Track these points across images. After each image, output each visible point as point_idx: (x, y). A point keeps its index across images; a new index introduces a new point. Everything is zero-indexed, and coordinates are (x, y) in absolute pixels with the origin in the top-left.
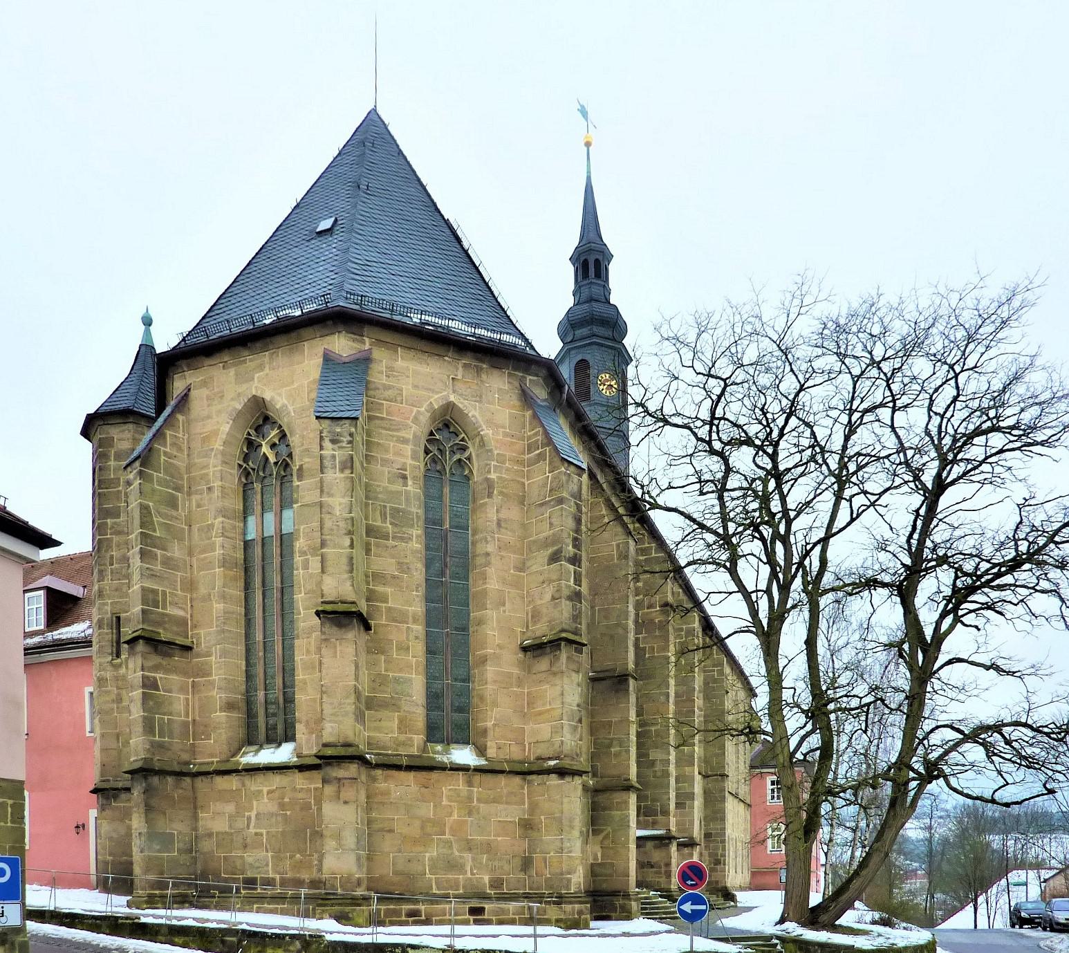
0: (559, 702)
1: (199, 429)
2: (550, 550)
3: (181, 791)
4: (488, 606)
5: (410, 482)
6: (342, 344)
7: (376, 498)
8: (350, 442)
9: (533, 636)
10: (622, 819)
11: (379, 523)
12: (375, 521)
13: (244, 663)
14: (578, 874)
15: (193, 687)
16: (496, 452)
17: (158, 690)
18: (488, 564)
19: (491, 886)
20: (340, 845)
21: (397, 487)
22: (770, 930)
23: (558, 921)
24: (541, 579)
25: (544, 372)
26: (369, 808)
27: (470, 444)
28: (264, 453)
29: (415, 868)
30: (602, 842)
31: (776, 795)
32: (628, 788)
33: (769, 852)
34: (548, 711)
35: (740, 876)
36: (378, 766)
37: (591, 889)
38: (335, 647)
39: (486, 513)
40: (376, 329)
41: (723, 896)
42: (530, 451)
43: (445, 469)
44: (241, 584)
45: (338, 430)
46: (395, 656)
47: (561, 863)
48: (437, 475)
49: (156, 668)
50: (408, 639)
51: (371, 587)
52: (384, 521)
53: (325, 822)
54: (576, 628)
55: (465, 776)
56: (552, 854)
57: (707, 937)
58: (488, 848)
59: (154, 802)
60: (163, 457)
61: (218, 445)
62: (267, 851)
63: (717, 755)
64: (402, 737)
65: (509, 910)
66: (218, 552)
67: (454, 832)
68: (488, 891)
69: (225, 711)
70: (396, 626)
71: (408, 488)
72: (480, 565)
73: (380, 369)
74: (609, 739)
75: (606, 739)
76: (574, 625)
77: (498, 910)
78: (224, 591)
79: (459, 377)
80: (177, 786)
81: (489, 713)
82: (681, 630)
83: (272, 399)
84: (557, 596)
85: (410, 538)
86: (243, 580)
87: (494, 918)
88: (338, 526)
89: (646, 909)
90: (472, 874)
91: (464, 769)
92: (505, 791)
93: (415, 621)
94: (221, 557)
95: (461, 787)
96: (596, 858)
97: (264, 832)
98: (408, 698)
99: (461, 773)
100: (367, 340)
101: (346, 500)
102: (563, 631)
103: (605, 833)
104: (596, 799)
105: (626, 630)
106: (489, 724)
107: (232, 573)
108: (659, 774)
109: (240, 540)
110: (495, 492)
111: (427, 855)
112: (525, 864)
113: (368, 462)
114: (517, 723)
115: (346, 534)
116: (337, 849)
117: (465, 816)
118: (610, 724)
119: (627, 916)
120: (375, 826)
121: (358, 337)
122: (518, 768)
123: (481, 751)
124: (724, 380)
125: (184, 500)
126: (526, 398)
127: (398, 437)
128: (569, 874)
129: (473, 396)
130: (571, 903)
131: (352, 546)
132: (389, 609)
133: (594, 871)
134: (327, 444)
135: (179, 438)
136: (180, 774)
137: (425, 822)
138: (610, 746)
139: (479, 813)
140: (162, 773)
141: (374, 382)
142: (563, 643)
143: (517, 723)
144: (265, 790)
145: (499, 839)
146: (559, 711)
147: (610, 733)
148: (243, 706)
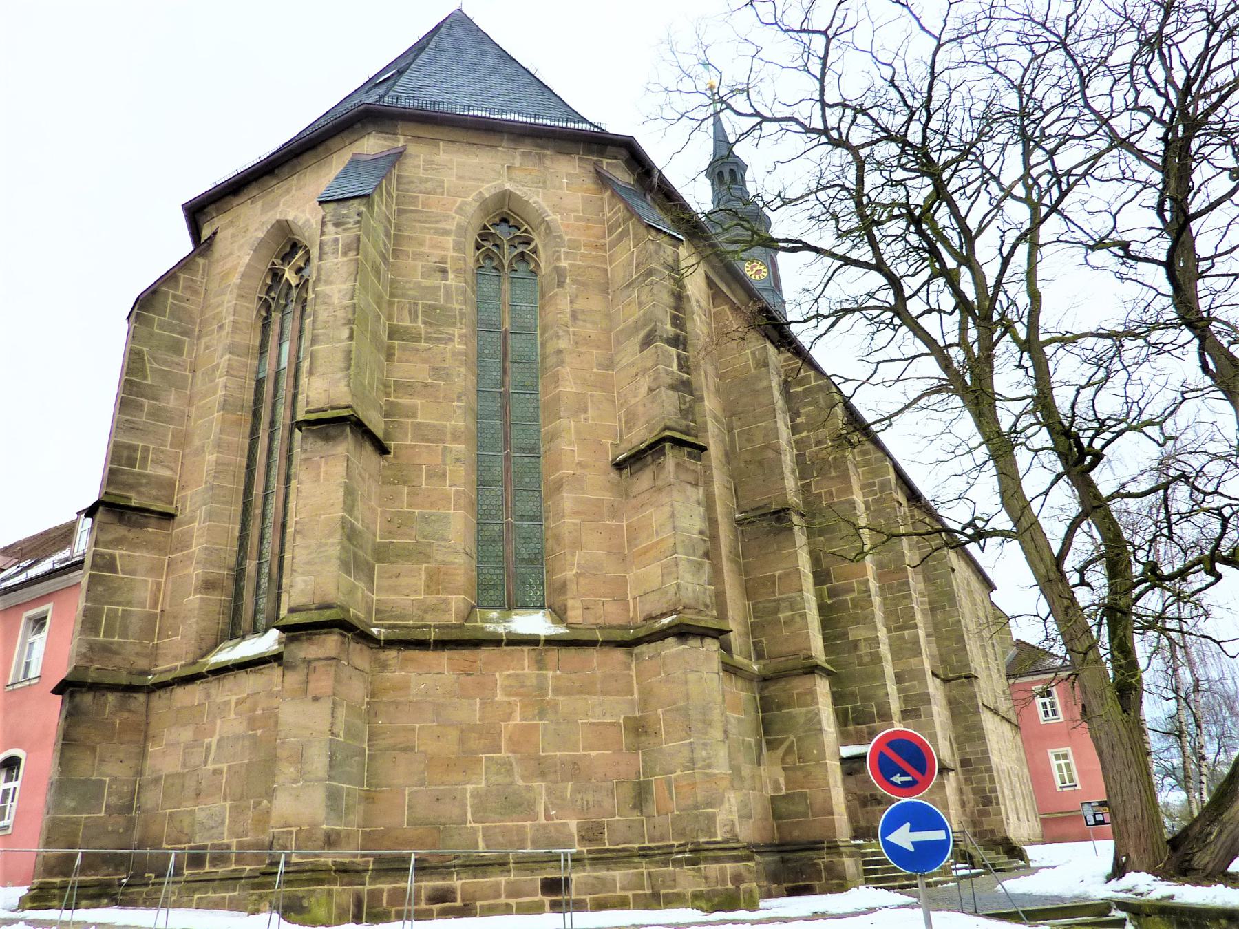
0: (669, 527)
1: (218, 269)
2: (642, 334)
3: (126, 715)
4: (562, 414)
5: (451, 276)
6: (371, 145)
7: (404, 295)
8: (358, 222)
9: (629, 447)
10: (810, 720)
12: (402, 320)
13: (238, 527)
14: (726, 805)
15: (168, 566)
16: (566, 238)
17: (115, 571)
18: (561, 363)
19: (583, 839)
20: (301, 772)
21: (435, 281)
22: (1102, 891)
23: (696, 896)
24: (633, 371)
25: (624, 153)
26: (372, 711)
27: (534, 236)
28: (287, 279)
29: (449, 811)
30: (783, 760)
31: (1049, 707)
32: (812, 669)
33: (1059, 790)
34: (657, 543)
35: (1025, 825)
36: (390, 644)
37: (777, 842)
38: (319, 467)
39: (557, 305)
40: (411, 125)
41: (1006, 852)
42: (610, 233)
43: (503, 264)
44: (247, 430)
45: (345, 211)
46: (424, 486)
47: (693, 785)
48: (494, 272)
49: (117, 543)
50: (444, 462)
51: (392, 399)
53: (282, 734)
54: (688, 426)
55: (534, 654)
56: (679, 773)
57: (975, 913)
58: (575, 770)
59: (79, 732)
60: (170, 300)
61: (235, 279)
62: (225, 799)
63: (956, 651)
64: (432, 599)
65: (614, 880)
66: (221, 392)
67: (514, 746)
69: (200, 593)
70: (428, 446)
71: (448, 282)
72: (552, 366)
73: (416, 163)
74: (775, 601)
75: (770, 601)
76: (684, 423)
77: (590, 880)
78: (220, 438)
79: (517, 165)
80: (122, 707)
81: (569, 557)
82: (873, 484)
83: (296, 217)
84: (654, 386)
85: (450, 339)
86: (249, 425)
87: (588, 898)
88: (335, 316)
89: (874, 872)
90: (548, 817)
91: (531, 641)
92: (599, 673)
93: (456, 438)
94: (222, 400)
95: (526, 671)
96: (777, 788)
97: (224, 766)
98: (443, 543)
99: (526, 649)
100: (401, 138)
101: (347, 286)
102: (667, 428)
103: (785, 745)
104: (766, 693)
105: (777, 451)
106: (570, 574)
107: (233, 417)
108: (866, 659)
109: (250, 379)
110: (568, 281)
111: (469, 787)
112: (640, 794)
113: (396, 257)
114: (613, 570)
115: (344, 325)
116: (295, 781)
117: (533, 718)
118: (772, 579)
119: (839, 885)
120: (381, 743)
121: (391, 136)
122: (618, 635)
123: (559, 615)
124: (824, 33)
125: (191, 345)
126: (603, 181)
127: (436, 229)
128: (709, 804)
129: (533, 183)
130: (717, 860)
131: (351, 337)
132: (418, 426)
133: (778, 808)
134: (330, 228)
135: (196, 281)
136: (130, 689)
137: (465, 731)
138: (777, 610)
139: (556, 712)
140: (97, 687)
141: (408, 177)
142: (667, 445)
143: (613, 570)
144: (234, 699)
145: (593, 753)
146: (671, 541)
147: (774, 592)
148: (230, 584)
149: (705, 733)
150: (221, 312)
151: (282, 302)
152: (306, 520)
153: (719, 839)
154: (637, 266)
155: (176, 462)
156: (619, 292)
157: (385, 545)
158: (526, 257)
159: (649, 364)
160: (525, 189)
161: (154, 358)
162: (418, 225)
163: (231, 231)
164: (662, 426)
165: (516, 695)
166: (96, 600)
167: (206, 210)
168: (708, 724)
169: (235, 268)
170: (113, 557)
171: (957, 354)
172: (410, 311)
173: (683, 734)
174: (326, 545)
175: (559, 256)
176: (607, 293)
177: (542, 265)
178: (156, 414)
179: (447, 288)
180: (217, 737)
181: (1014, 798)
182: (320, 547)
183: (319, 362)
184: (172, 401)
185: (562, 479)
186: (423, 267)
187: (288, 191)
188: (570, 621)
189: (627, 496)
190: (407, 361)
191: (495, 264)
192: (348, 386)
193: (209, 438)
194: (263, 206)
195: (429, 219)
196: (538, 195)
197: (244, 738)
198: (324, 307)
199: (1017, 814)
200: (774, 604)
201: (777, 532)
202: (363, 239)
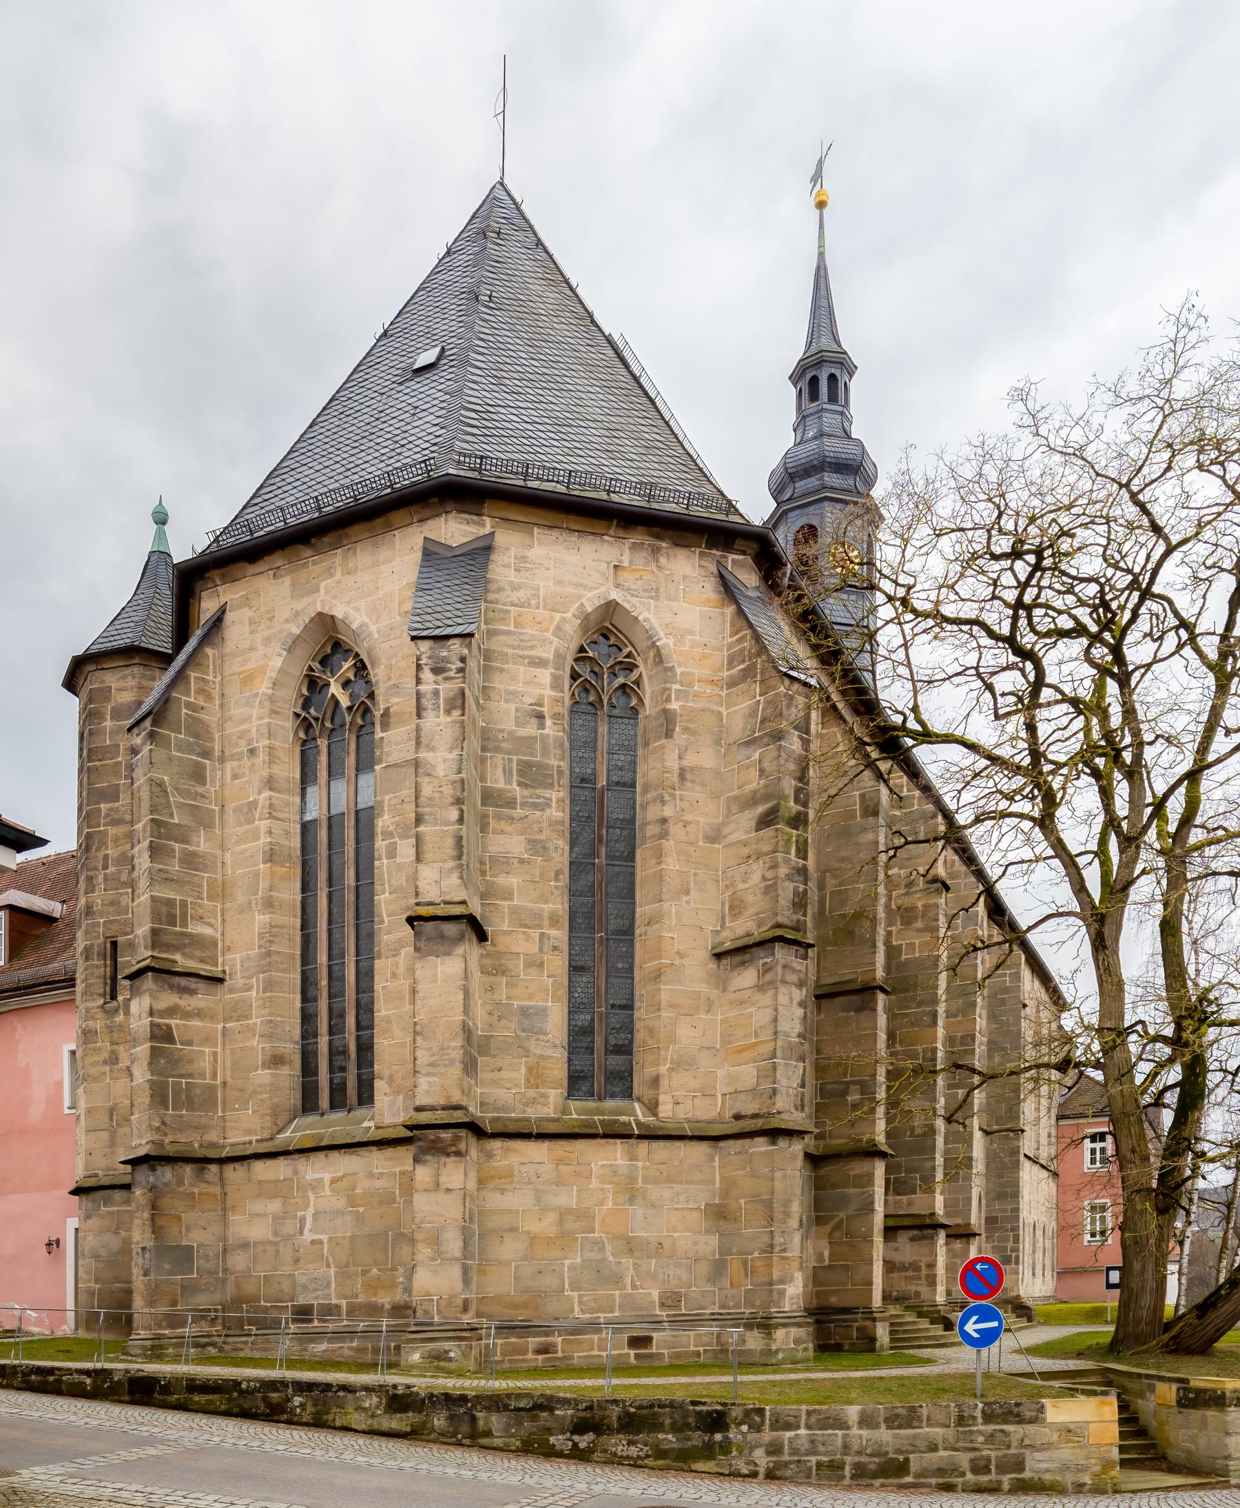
2: (761, 809)
5: (548, 723)
8: (461, 670)
11: (501, 784)
16: (679, 671)
24: (745, 851)
28: (333, 695)
32: (873, 1153)
34: (755, 1045)
40: (500, 504)
43: (601, 700)
49: (172, 1011)
52: (509, 782)
53: (417, 1220)
56: (756, 1254)
64: (531, 1093)
68: (658, 1313)
71: (545, 732)
81: (662, 1052)
88: (441, 792)
90: (634, 1287)
94: (267, 848)
97: (324, 1238)
98: (541, 1037)
99: (619, 1141)
100: (487, 520)
102: (778, 926)
108: (918, 1131)
110: (677, 729)
111: (567, 1262)
115: (452, 804)
116: (433, 1259)
117: (624, 1203)
121: (474, 517)
126: (728, 589)
127: (530, 657)
128: (782, 1282)
131: (461, 820)
132: (514, 910)
134: (427, 675)
135: (208, 682)
138: (845, 1093)
144: (327, 1177)
149: (784, 1223)
150: (249, 731)
151: (328, 724)
152: (426, 1021)
153: (786, 1309)
154: (762, 722)
155: (215, 917)
156: (735, 747)
157: (488, 1038)
158: (628, 690)
159: (766, 848)
160: (634, 600)
161: (177, 789)
162: (510, 651)
163: (247, 613)
164: (774, 922)
165: (610, 1183)
166: (160, 1074)
167: (207, 575)
168: (787, 1214)
169: (262, 670)
170: (169, 1027)
171: (1092, 877)
172: (504, 769)
173: (765, 1223)
174: (448, 1048)
175: (670, 695)
176: (720, 745)
177: (647, 701)
178: (191, 860)
179: (544, 738)
180: (311, 1210)
181: (1034, 1252)
182: (442, 1049)
183: (427, 847)
184: (202, 844)
185: (660, 969)
186: (517, 710)
187: (329, 573)
188: (660, 1115)
189: (725, 990)
190: (502, 832)
191: (592, 698)
192: (461, 878)
193: (256, 894)
194: (293, 585)
195: (523, 644)
196: (649, 610)
197: (343, 1214)
198: (427, 779)
199: (1034, 1269)
200: (843, 1086)
201: (858, 1010)
202: (467, 691)
